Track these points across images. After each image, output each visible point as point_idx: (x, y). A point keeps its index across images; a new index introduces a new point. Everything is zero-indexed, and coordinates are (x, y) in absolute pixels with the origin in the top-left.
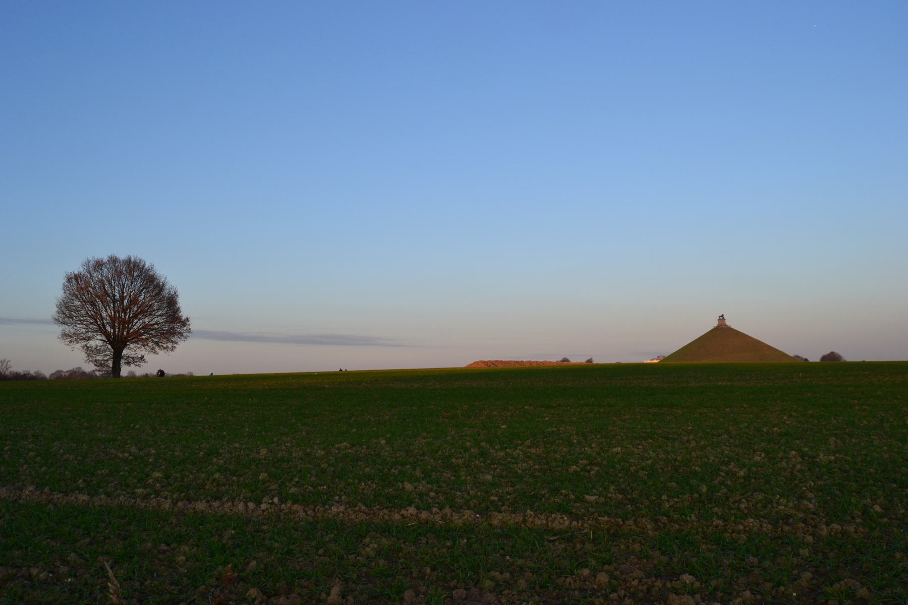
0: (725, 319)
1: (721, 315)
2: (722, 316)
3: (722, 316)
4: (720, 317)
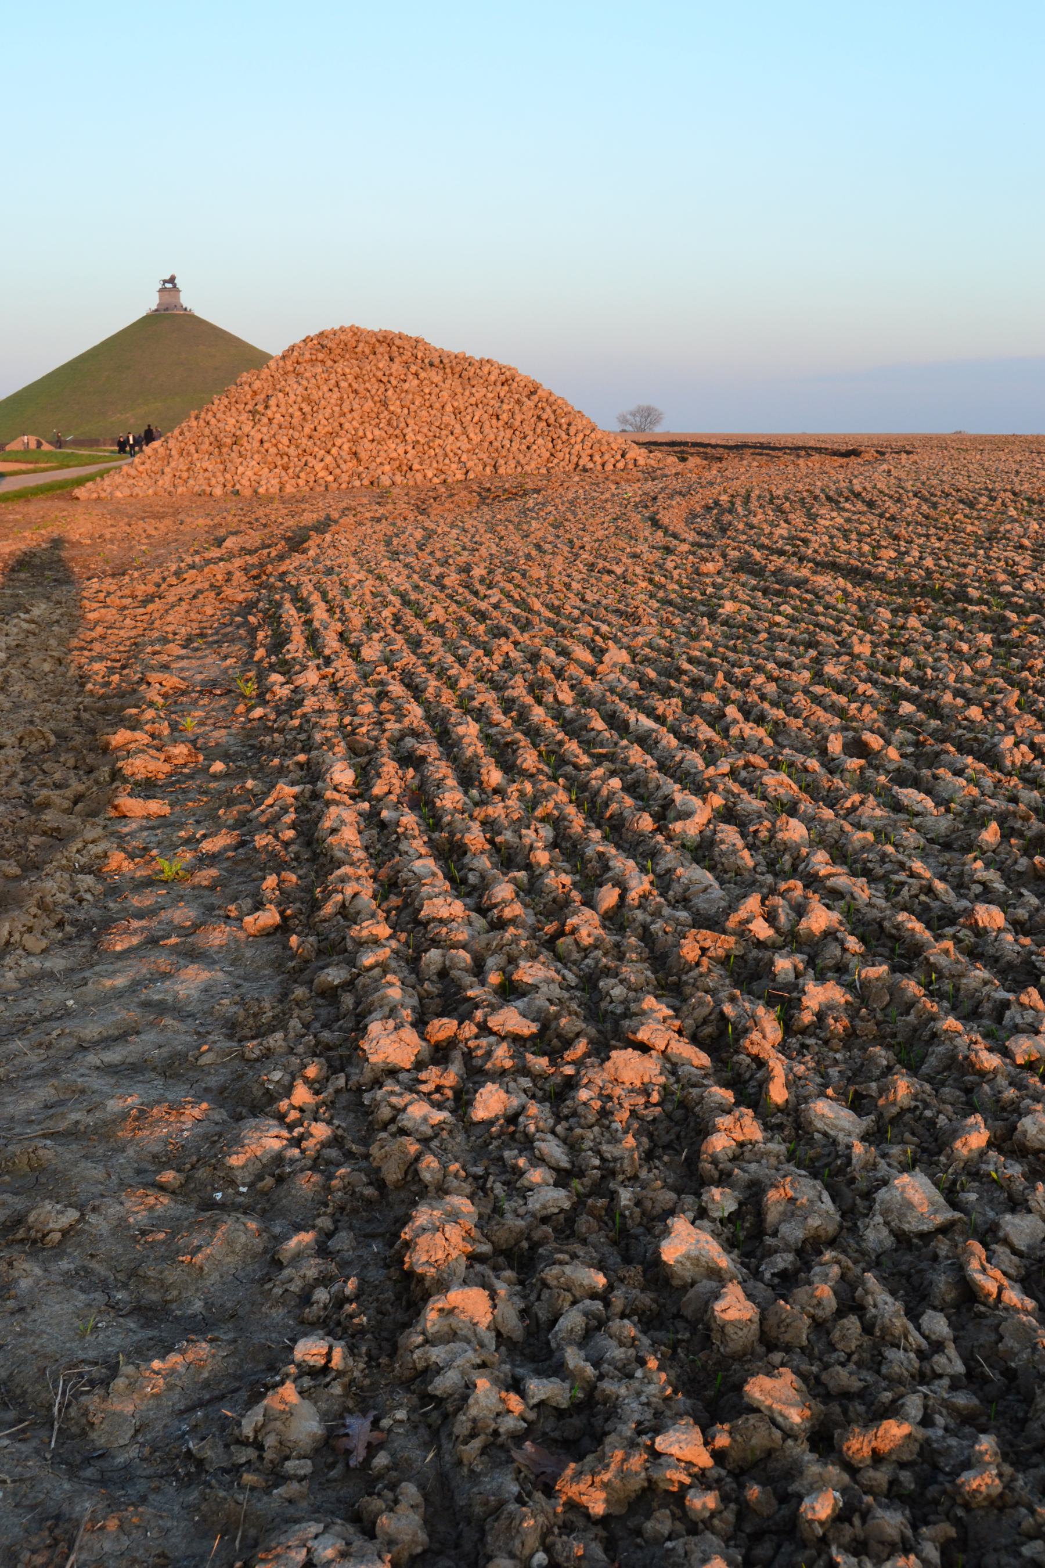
0: (178, 291)
1: (167, 278)
2: (172, 280)
3: (172, 280)
4: (165, 282)
